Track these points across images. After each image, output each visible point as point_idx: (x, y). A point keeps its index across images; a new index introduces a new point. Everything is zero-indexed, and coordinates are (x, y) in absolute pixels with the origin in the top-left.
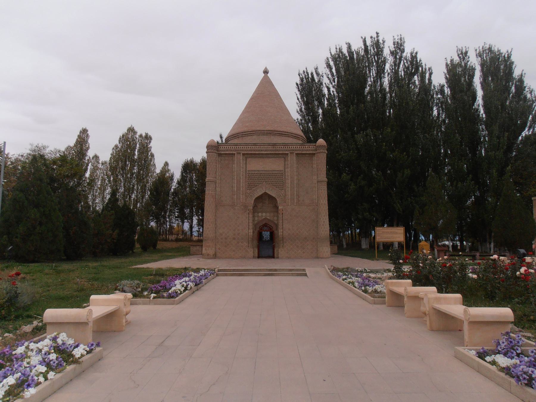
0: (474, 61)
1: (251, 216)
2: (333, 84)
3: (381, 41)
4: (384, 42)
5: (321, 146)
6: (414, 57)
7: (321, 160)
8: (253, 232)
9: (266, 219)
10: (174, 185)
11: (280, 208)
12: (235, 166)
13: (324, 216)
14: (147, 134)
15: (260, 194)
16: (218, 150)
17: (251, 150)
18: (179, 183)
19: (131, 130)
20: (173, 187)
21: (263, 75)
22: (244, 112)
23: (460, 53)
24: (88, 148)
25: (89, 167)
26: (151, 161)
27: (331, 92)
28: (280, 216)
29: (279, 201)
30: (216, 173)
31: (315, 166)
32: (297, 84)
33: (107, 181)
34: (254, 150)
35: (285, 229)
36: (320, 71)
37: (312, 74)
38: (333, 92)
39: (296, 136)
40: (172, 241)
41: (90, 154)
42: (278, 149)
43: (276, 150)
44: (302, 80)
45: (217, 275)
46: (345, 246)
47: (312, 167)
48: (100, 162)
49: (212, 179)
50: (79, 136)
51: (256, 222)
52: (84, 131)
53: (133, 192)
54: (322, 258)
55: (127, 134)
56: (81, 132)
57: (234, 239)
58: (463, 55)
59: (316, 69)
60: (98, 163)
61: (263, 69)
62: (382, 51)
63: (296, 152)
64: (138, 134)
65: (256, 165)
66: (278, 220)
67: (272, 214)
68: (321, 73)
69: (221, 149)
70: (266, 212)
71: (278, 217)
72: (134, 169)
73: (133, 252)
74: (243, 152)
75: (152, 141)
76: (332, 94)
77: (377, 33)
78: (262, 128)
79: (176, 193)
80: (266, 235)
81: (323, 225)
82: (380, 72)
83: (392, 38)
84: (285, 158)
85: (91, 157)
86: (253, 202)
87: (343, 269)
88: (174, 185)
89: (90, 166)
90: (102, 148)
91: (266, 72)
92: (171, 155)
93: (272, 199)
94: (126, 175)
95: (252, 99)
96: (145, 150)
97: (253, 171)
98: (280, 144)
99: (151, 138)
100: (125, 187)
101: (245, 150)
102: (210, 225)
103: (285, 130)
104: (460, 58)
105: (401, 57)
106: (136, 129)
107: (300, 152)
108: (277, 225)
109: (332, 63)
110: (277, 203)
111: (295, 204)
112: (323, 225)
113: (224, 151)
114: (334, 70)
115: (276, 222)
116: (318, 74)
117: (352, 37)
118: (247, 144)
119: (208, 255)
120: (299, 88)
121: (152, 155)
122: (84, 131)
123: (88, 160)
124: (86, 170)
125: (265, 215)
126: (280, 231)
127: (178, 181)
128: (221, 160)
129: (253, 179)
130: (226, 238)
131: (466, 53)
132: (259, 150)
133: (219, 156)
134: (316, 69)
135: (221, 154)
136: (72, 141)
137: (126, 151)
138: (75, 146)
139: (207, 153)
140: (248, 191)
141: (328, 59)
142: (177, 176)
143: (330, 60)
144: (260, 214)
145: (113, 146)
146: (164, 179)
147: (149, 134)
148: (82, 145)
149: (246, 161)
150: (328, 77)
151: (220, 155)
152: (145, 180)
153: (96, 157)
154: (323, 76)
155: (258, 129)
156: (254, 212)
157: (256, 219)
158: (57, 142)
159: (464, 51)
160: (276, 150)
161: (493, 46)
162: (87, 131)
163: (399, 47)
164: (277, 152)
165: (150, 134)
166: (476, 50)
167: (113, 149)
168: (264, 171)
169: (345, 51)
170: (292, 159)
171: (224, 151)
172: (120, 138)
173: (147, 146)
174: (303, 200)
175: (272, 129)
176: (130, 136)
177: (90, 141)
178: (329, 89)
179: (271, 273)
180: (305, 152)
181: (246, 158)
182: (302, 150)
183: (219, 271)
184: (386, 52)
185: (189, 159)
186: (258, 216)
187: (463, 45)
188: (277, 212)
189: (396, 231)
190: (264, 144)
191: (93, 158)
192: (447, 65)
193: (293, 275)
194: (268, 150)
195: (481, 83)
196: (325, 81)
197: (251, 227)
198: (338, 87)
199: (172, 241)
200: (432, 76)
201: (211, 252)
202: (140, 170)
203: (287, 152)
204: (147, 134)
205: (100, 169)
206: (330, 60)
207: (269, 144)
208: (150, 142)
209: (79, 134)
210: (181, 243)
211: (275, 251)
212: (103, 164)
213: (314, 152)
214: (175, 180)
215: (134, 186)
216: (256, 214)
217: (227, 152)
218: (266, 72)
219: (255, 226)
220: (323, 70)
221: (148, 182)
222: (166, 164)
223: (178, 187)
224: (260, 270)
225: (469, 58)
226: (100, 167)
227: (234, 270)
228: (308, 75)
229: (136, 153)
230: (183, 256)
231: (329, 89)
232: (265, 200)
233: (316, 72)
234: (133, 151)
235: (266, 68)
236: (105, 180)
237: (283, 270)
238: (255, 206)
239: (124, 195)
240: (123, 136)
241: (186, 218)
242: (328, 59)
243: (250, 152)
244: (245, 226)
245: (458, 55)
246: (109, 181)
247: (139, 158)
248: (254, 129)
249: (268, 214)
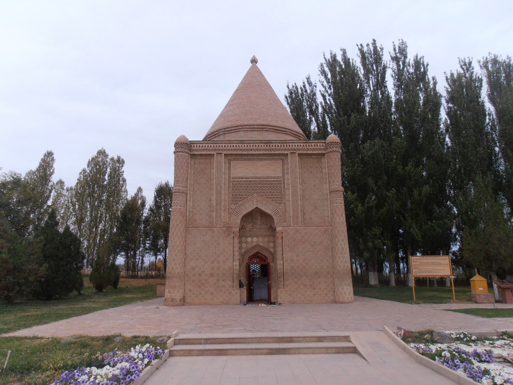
0: (478, 72)
1: (236, 241)
2: (329, 91)
4: (382, 49)
5: (333, 143)
6: (418, 63)
8: (240, 265)
9: (257, 245)
10: (146, 212)
11: (278, 229)
12: (214, 171)
13: (343, 240)
14: (119, 158)
15: (250, 209)
16: (190, 150)
17: (235, 150)
18: (151, 210)
19: (102, 153)
20: (145, 215)
21: (251, 65)
22: (227, 106)
23: (462, 64)
24: (52, 174)
25: (52, 194)
26: (122, 186)
27: (327, 100)
28: (279, 241)
29: (276, 219)
30: (187, 181)
31: (325, 171)
32: (286, 97)
33: (71, 210)
34: (241, 150)
35: (285, 261)
36: (312, 80)
38: (329, 100)
40: (141, 277)
41: (54, 179)
42: (274, 147)
43: (270, 150)
44: (291, 93)
45: (171, 354)
47: (321, 172)
48: (65, 188)
49: (180, 188)
50: (43, 160)
51: (243, 251)
52: (50, 154)
53: (100, 222)
54: (342, 303)
55: (96, 157)
56: (45, 155)
57: (212, 275)
59: (308, 79)
60: (63, 189)
61: (250, 58)
62: (380, 59)
63: (299, 152)
64: (110, 157)
65: (242, 170)
66: (275, 247)
67: (266, 239)
68: (313, 83)
69: (195, 148)
70: (258, 237)
71: (274, 242)
72: (103, 196)
73: (80, 294)
74: (225, 152)
75: (125, 165)
76: (328, 102)
77: (374, 41)
78: (251, 122)
79: (147, 220)
80: (256, 267)
81: (342, 253)
83: (392, 44)
84: (283, 161)
85: (55, 183)
86: (239, 221)
87: (422, 334)
88: (146, 212)
89: (53, 194)
90: (68, 173)
91: (254, 61)
93: (266, 217)
94: (94, 202)
96: (117, 176)
97: (239, 178)
98: (276, 142)
99: (123, 162)
100: (91, 215)
101: (228, 150)
102: (176, 255)
103: (282, 126)
104: (463, 69)
105: (404, 63)
106: (107, 152)
107: (305, 152)
108: (274, 255)
110: (273, 222)
111: (300, 224)
112: (342, 253)
113: (200, 150)
114: (329, 76)
115: (272, 250)
116: (310, 84)
118: (230, 142)
119: (173, 300)
120: (288, 102)
121: (124, 181)
122: (50, 154)
123: (52, 186)
124: (48, 197)
125: (256, 241)
126: (279, 262)
127: (150, 207)
128: (195, 163)
129: (239, 189)
130: (200, 275)
131: (470, 63)
132: (247, 150)
133: (191, 158)
134: (308, 79)
135: (194, 155)
136: (34, 165)
138: (38, 170)
139: (175, 153)
140: (233, 206)
141: (322, 65)
142: (150, 201)
143: (325, 66)
144: (249, 240)
145: (80, 170)
146: (134, 206)
148: (45, 169)
149: (229, 163)
150: (323, 85)
152: (115, 208)
153: (61, 183)
154: (316, 87)
155: (246, 123)
156: (240, 237)
157: (244, 245)
159: (467, 61)
160: (270, 150)
161: (499, 56)
162: (53, 154)
164: (273, 152)
165: (122, 157)
166: (479, 62)
167: (80, 173)
168: (254, 178)
169: (339, 58)
170: (293, 161)
171: (200, 150)
172: (89, 162)
173: (119, 169)
174: (311, 219)
175: (264, 123)
176: (100, 159)
177: (55, 165)
179: (282, 347)
180: (311, 152)
181: (230, 161)
182: (308, 150)
183: (177, 342)
185: (164, 183)
186: (247, 242)
187: (465, 56)
188: (274, 236)
189: (440, 261)
190: (255, 142)
191: (57, 183)
192: (447, 79)
193: (327, 351)
194: (260, 150)
195: (489, 96)
197: (237, 257)
198: (336, 96)
199: (141, 277)
200: (437, 86)
201: (178, 295)
202: (110, 196)
203: (286, 152)
204: (119, 158)
205: (65, 196)
206: (325, 66)
207: (261, 142)
208: (122, 166)
209: (43, 157)
210: (151, 281)
211: (272, 292)
212: (67, 190)
213: (323, 152)
214: (147, 207)
215: (101, 215)
216: (244, 239)
217: (203, 153)
218: (254, 61)
219: (242, 255)
220: (317, 79)
221: (117, 210)
222: (140, 190)
223: (151, 214)
224: (260, 340)
225: (473, 69)
226: (65, 193)
227: (207, 341)
228: (298, 90)
229: (106, 177)
230: (148, 298)
231: (324, 97)
232: (256, 215)
233: (308, 82)
234: (103, 177)
235: (254, 57)
236: (69, 208)
237: (305, 339)
238: (242, 228)
239: (90, 226)
240: (93, 159)
241: (159, 251)
242: (322, 65)
243: (235, 152)
244: (227, 258)
245: (461, 67)
246: (74, 209)
247: (109, 184)
249: (261, 239)
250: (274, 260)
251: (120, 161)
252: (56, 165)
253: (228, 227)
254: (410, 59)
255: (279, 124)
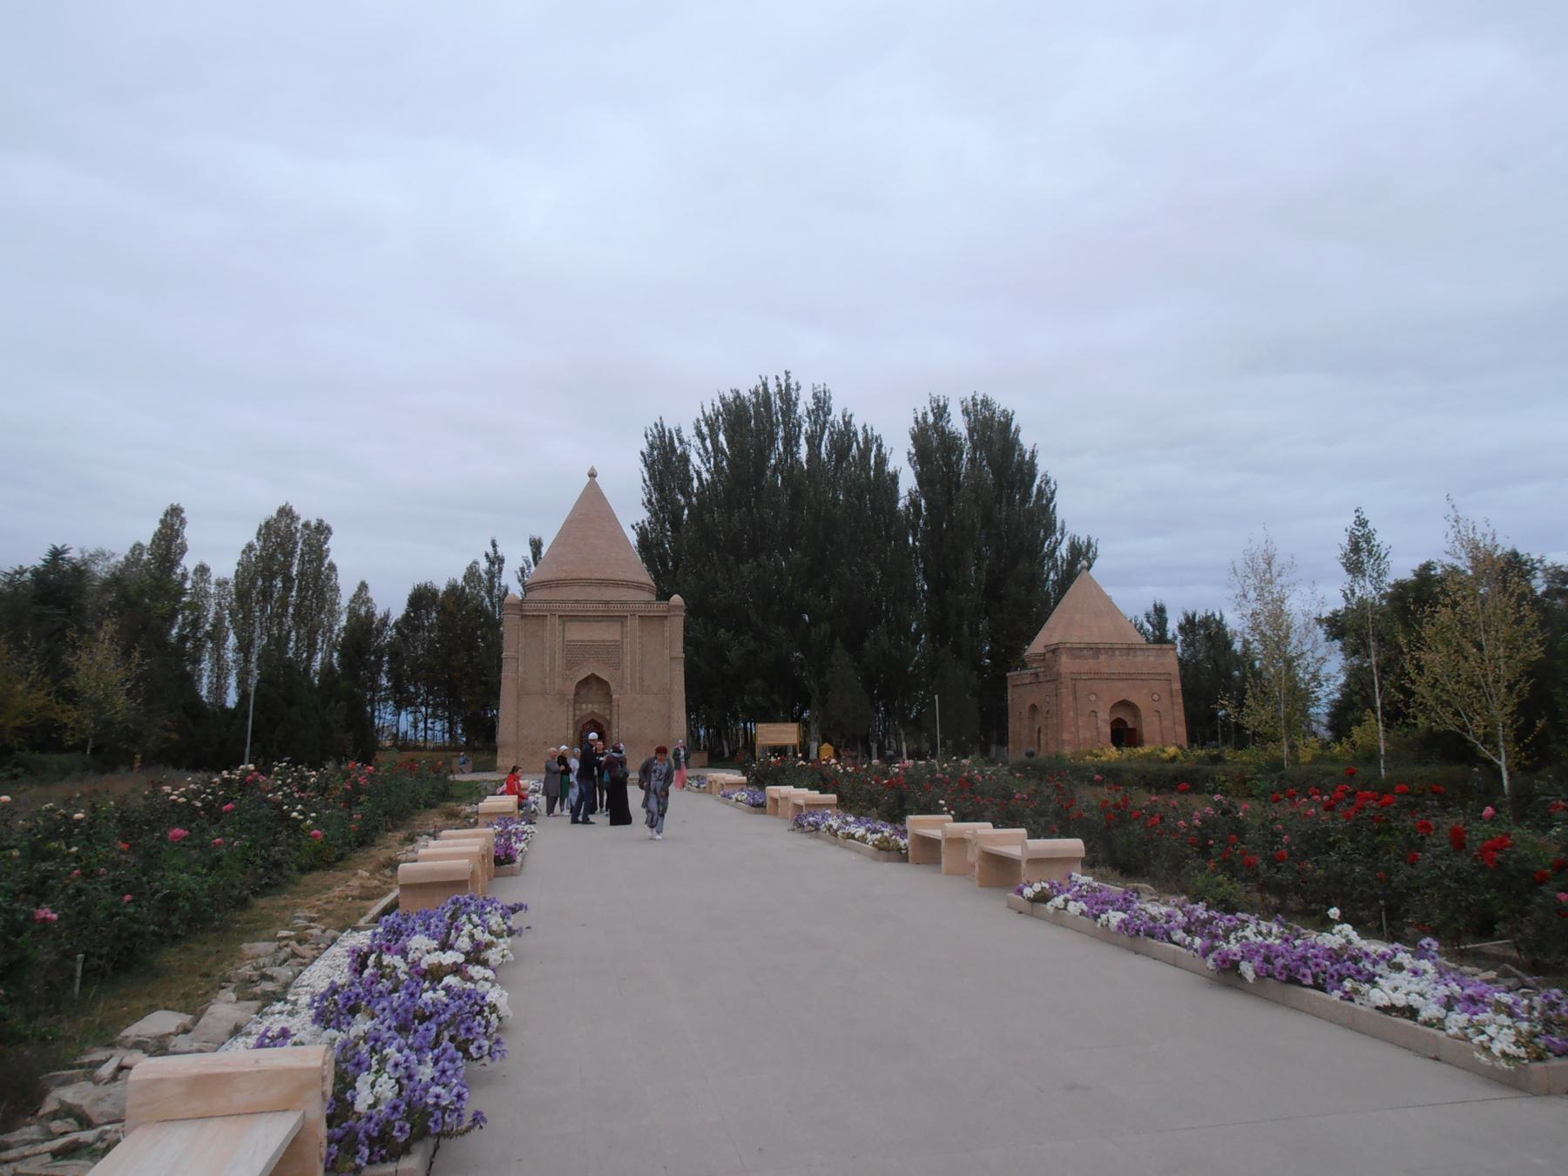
3: (793, 386)
5: (677, 607)
7: (676, 627)
14: (320, 522)
19: (286, 513)
24: (183, 550)
29: (613, 686)
37: (671, 438)
39: (640, 586)
41: (189, 563)
44: (652, 447)
46: (727, 754)
48: (213, 579)
52: (175, 513)
58: (941, 411)
59: (679, 431)
64: (302, 521)
65: (579, 633)
77: (787, 373)
82: (791, 441)
90: (217, 552)
91: (592, 475)
92: (381, 569)
95: (569, 522)
99: (330, 532)
105: (825, 422)
106: (297, 510)
108: (609, 723)
109: (705, 430)
116: (681, 441)
117: (743, 378)
121: (332, 567)
122: (175, 513)
125: (591, 708)
126: (615, 730)
129: (574, 654)
136: (146, 531)
137: (272, 557)
145: (243, 547)
147: (326, 522)
151: (523, 617)
153: (202, 570)
158: (111, 535)
163: (822, 405)
170: (633, 624)
178: (699, 474)
184: (801, 410)
196: (695, 460)
204: (320, 522)
207: (599, 602)
208: (327, 539)
218: (592, 475)
219: (576, 723)
222: (363, 587)
234: (289, 558)
238: (577, 694)
248: (575, 576)
250: (609, 727)
251: (322, 530)
252: (190, 534)
253: (562, 695)
254: (836, 416)
255: (620, 575)
